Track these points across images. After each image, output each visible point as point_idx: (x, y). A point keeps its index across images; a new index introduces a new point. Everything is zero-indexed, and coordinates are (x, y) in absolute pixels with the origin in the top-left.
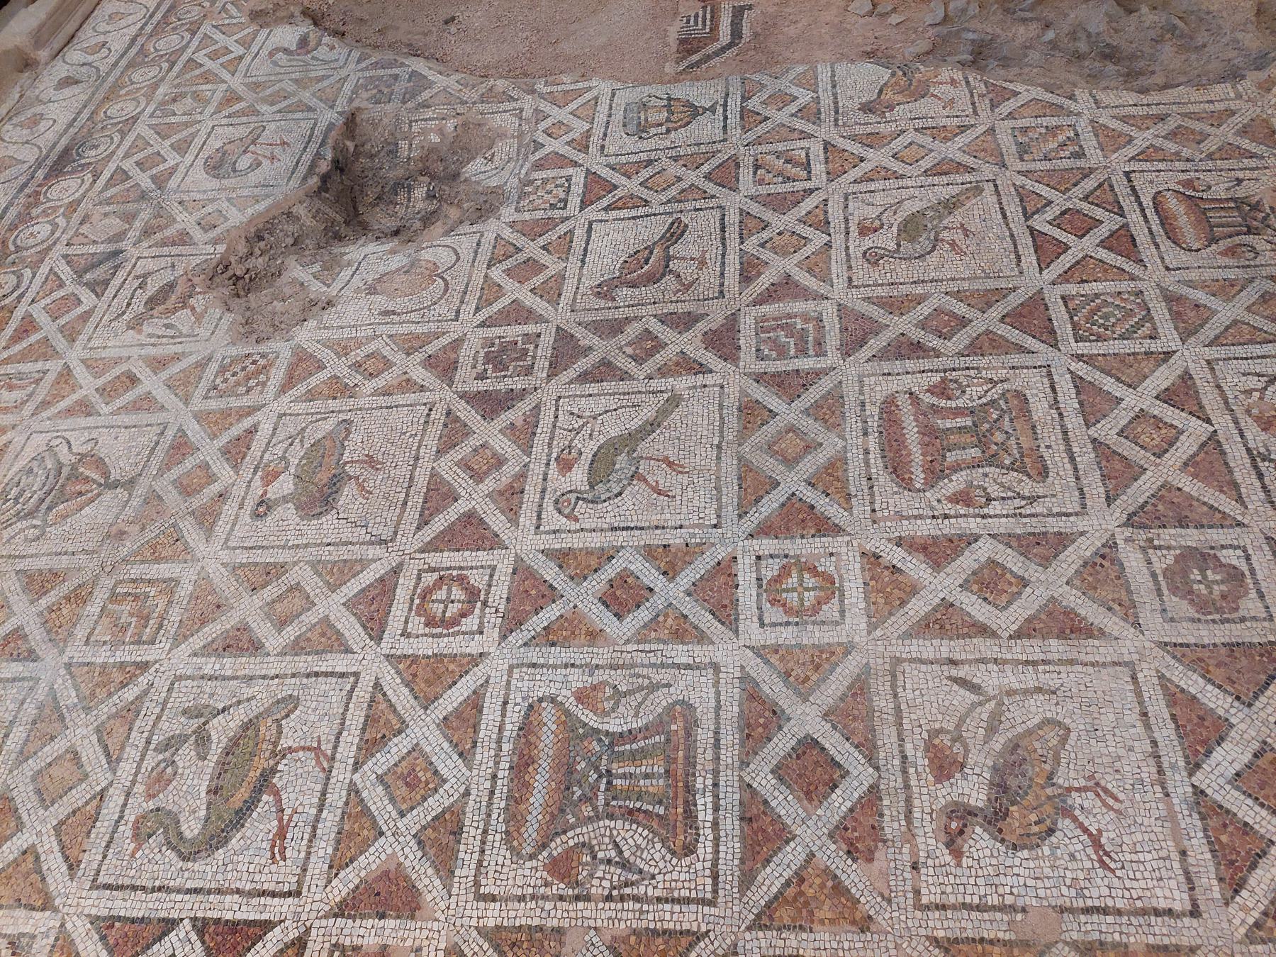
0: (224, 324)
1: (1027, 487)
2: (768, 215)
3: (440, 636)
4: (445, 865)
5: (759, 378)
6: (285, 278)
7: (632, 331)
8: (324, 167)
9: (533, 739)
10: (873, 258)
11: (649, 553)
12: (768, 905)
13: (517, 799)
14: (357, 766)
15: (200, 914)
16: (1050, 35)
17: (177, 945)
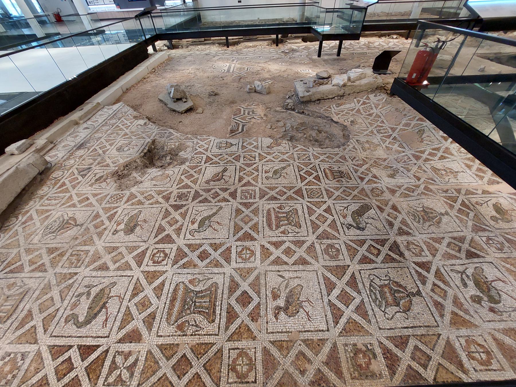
0: (114, 186)
1: (297, 230)
2: (246, 168)
3: (156, 266)
4: (149, 327)
5: (241, 204)
6: (132, 176)
7: (213, 191)
8: (145, 151)
9: (177, 293)
10: (267, 178)
11: (211, 245)
12: (231, 335)
13: (170, 309)
14: (130, 301)
15: (80, 344)
16: (305, 136)
17: (72, 353)
